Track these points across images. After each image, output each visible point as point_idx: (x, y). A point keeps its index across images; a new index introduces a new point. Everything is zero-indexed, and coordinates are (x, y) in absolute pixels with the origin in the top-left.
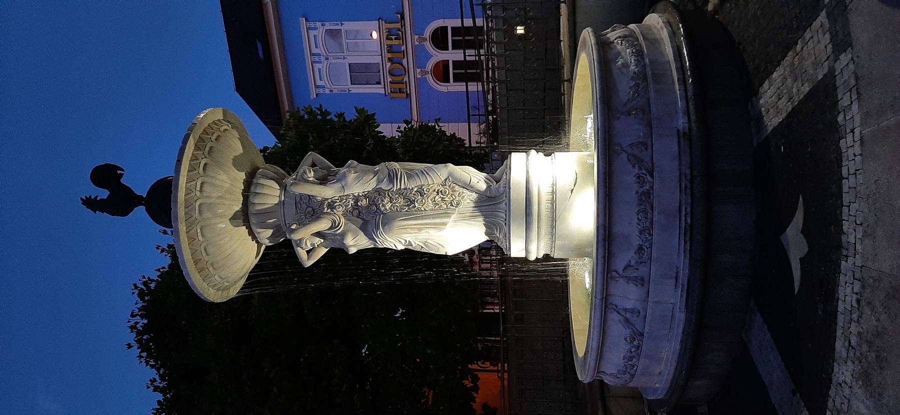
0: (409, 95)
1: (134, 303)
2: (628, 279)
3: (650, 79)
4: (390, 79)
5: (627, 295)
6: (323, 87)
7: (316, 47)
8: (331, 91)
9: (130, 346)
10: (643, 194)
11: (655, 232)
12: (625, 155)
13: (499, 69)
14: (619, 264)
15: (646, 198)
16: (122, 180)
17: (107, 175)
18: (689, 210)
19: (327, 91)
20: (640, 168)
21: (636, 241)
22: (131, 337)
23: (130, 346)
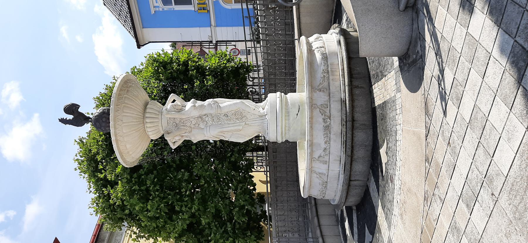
0: (209, 11)
1: (76, 148)
2: (321, 162)
3: (330, 73)
4: (197, 2)
5: (321, 168)
6: (158, 7)
7: (157, 3)
8: (163, 9)
9: (76, 169)
10: (326, 127)
11: (331, 142)
12: (318, 110)
13: (260, 10)
14: (316, 155)
15: (327, 128)
16: (80, 110)
17: (72, 109)
18: (345, 134)
19: (161, 9)
20: (325, 116)
21: (323, 146)
22: (76, 165)
23: (76, 169)
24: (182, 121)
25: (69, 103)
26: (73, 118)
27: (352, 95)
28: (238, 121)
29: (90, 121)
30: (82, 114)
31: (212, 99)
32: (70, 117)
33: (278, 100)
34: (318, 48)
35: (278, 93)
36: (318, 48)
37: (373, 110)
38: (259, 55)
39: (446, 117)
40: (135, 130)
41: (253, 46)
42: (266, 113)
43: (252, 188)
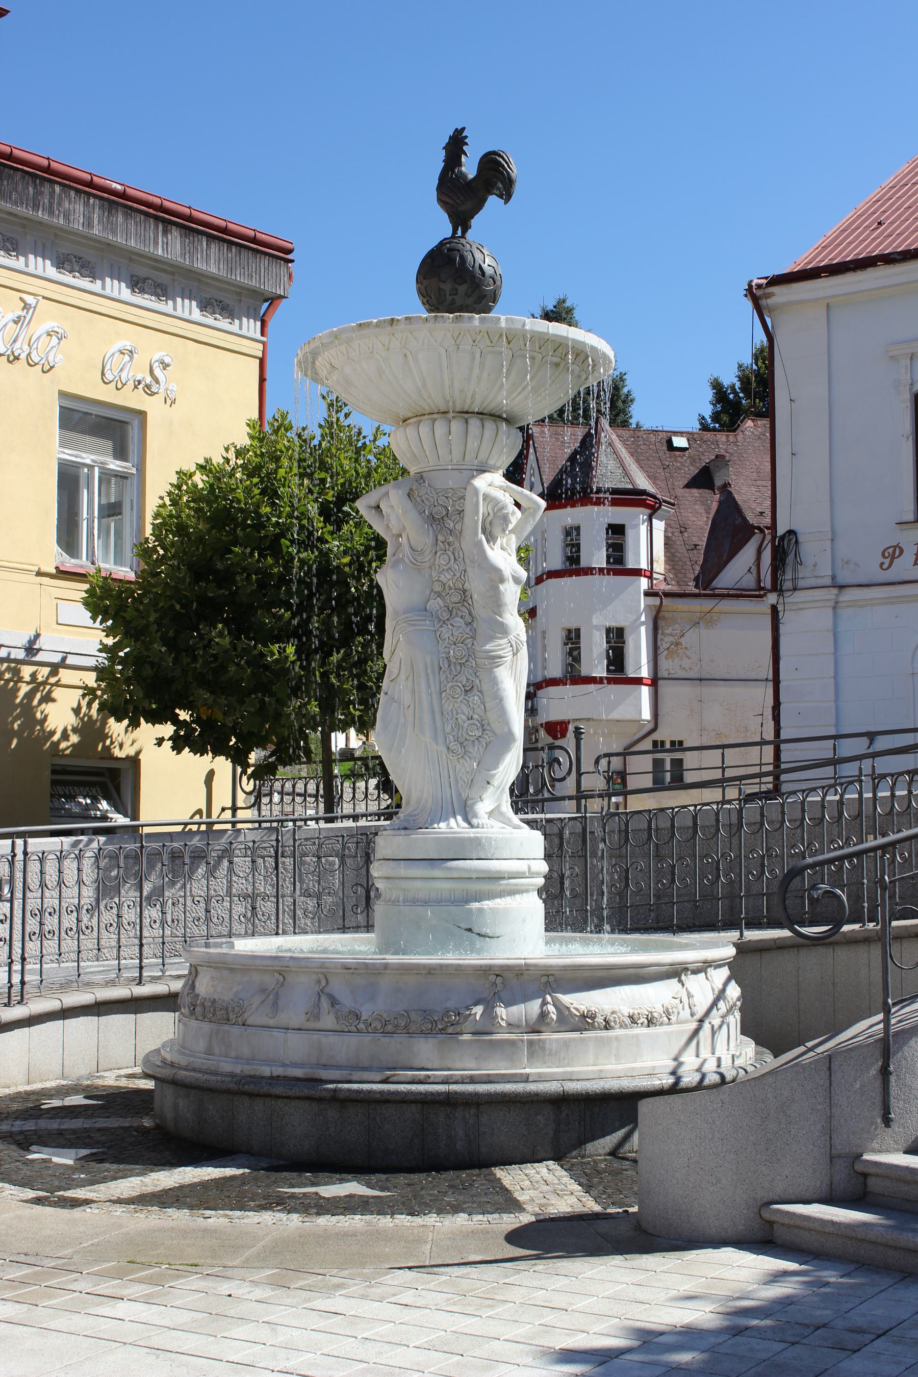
17: (495, 177)
24: (451, 539)
25: (515, 170)
26: (463, 175)
27: (508, 1102)
28: (448, 729)
29: (455, 231)
30: (479, 205)
31: (524, 637)
32: (469, 167)
33: (521, 866)
34: (690, 996)
35: (544, 867)
36: (690, 996)
37: (537, 1221)
38: (713, 795)
39: (367, 1296)
40: (424, 385)
41: (729, 773)
42: (475, 821)
43: (253, 757)
